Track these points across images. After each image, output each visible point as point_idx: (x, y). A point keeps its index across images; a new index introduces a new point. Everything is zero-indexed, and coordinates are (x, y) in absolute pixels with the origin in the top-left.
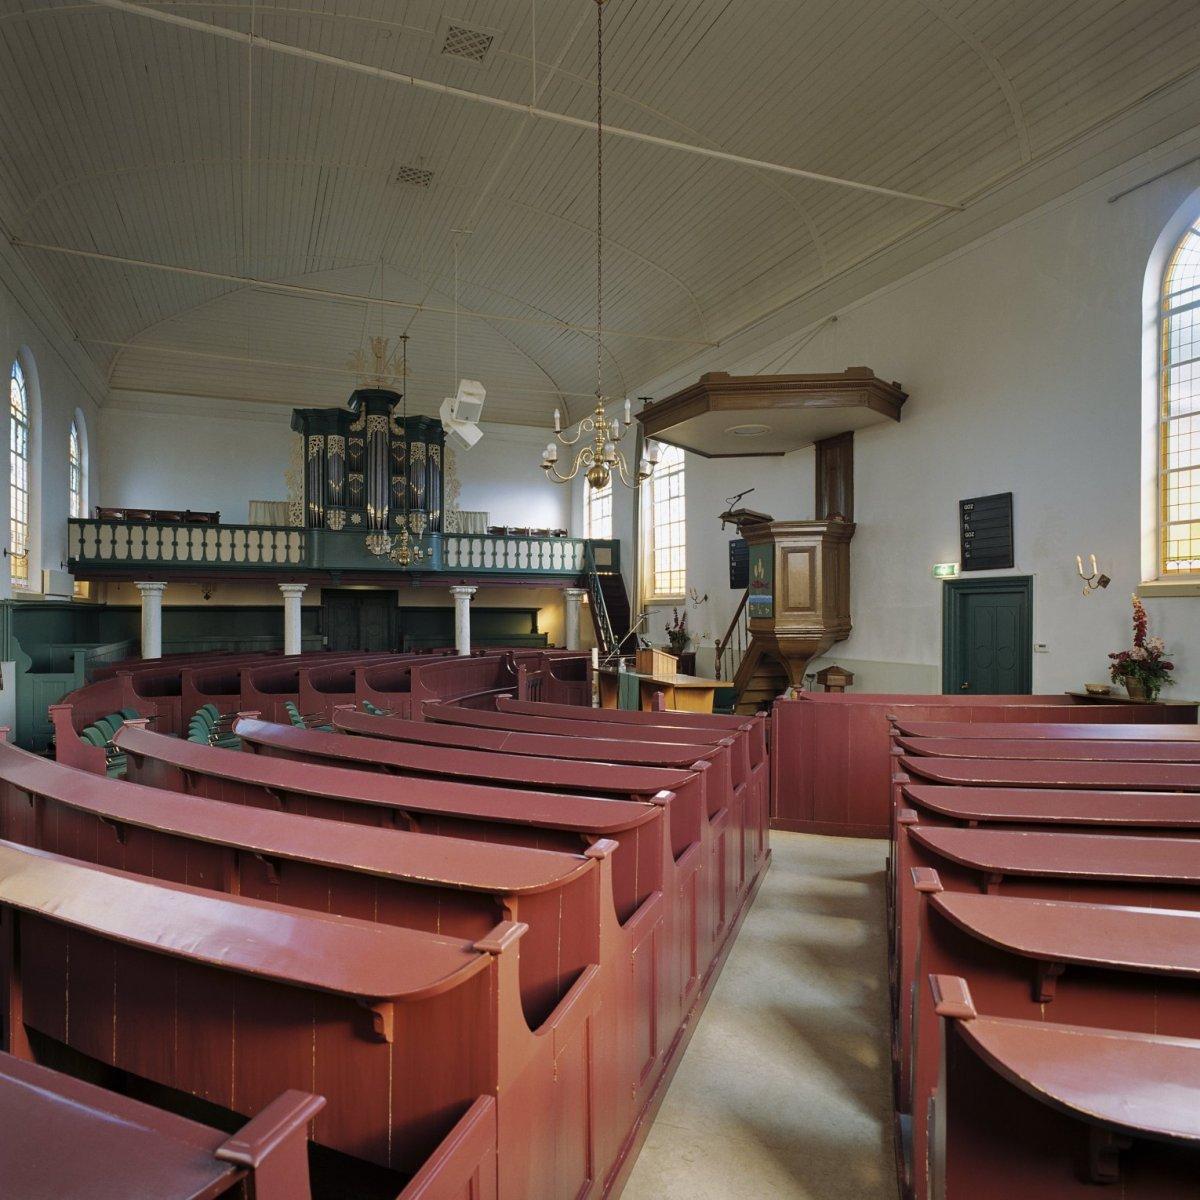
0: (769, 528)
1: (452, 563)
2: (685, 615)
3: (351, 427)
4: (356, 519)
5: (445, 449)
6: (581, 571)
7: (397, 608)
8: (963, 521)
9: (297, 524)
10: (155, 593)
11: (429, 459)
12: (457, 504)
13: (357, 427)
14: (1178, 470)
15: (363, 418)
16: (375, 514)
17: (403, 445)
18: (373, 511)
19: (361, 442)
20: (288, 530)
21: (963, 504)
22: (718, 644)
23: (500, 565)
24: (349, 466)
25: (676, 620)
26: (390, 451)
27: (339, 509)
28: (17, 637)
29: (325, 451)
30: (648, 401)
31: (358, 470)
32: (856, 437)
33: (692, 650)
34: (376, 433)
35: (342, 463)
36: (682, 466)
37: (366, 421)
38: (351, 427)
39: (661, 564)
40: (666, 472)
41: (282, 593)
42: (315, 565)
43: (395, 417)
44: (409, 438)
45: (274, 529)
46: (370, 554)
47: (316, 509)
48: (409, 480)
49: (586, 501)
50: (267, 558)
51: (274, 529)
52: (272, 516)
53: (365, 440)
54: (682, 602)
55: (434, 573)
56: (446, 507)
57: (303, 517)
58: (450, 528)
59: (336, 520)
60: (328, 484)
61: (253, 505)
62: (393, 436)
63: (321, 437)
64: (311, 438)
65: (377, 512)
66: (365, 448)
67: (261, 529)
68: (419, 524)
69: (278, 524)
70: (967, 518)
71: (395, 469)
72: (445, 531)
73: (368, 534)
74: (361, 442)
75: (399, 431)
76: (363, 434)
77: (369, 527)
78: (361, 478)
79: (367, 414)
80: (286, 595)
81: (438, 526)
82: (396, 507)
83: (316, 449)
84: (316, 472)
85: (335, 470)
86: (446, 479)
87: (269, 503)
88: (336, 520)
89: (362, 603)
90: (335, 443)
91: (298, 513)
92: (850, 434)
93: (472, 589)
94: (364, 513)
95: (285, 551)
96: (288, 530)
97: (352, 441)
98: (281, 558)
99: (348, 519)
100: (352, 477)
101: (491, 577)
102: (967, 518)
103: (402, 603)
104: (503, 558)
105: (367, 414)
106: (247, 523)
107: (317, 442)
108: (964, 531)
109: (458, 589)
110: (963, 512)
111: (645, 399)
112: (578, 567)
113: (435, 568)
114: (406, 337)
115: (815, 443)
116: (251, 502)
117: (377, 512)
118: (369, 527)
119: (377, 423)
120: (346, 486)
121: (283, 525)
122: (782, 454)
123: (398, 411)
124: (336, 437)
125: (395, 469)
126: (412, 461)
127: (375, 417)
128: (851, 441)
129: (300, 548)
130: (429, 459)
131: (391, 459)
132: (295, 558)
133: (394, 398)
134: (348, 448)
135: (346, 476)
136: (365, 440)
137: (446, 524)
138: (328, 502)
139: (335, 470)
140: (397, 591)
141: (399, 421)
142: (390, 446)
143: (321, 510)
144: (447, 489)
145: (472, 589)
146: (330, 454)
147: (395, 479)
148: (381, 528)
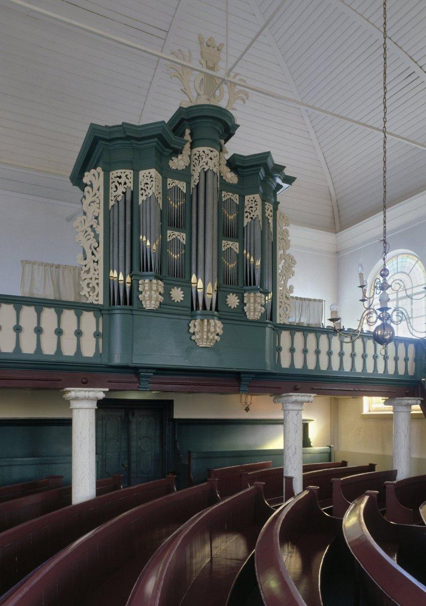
3: (171, 163)
4: (177, 294)
5: (278, 212)
9: (92, 299)
10: (261, 580)
12: (291, 288)
16: (204, 288)
17: (236, 198)
18: (200, 284)
19: (182, 186)
20: (79, 308)
24: (170, 220)
26: (220, 204)
28: (76, 186)
29: (134, 194)
31: (176, 224)
34: (206, 173)
37: (190, 156)
38: (171, 163)
41: (68, 403)
42: (117, 361)
44: (242, 189)
45: (59, 306)
47: (121, 277)
48: (242, 248)
50: (49, 349)
51: (59, 306)
52: (57, 288)
53: (188, 184)
56: (280, 288)
57: (100, 289)
60: (139, 242)
61: (28, 267)
62: (225, 185)
63: (130, 173)
64: (114, 174)
66: (188, 197)
67: (40, 304)
68: (255, 305)
69: (64, 299)
71: (230, 231)
73: (193, 317)
74: (182, 186)
75: (231, 177)
76: (185, 175)
78: (182, 237)
80: (74, 405)
81: (271, 314)
82: (225, 284)
83: (121, 189)
84: (121, 227)
85: (151, 220)
87: (52, 265)
89: (133, 415)
91: (93, 283)
94: (187, 286)
95: (75, 338)
96: (79, 308)
97: (172, 183)
98: (69, 350)
99: (167, 294)
103: (177, 415)
104: (326, 357)
106: (17, 292)
112: (411, 372)
116: (25, 263)
120: (164, 246)
121: (72, 299)
126: (246, 221)
127: (206, 149)
129: (97, 335)
132: (89, 350)
133: (85, 199)
134: (165, 191)
135: (163, 233)
136: (188, 184)
139: (151, 220)
140: (172, 401)
142: (220, 197)
143: (128, 279)
146: (141, 199)
147: (227, 244)
148: (211, 309)
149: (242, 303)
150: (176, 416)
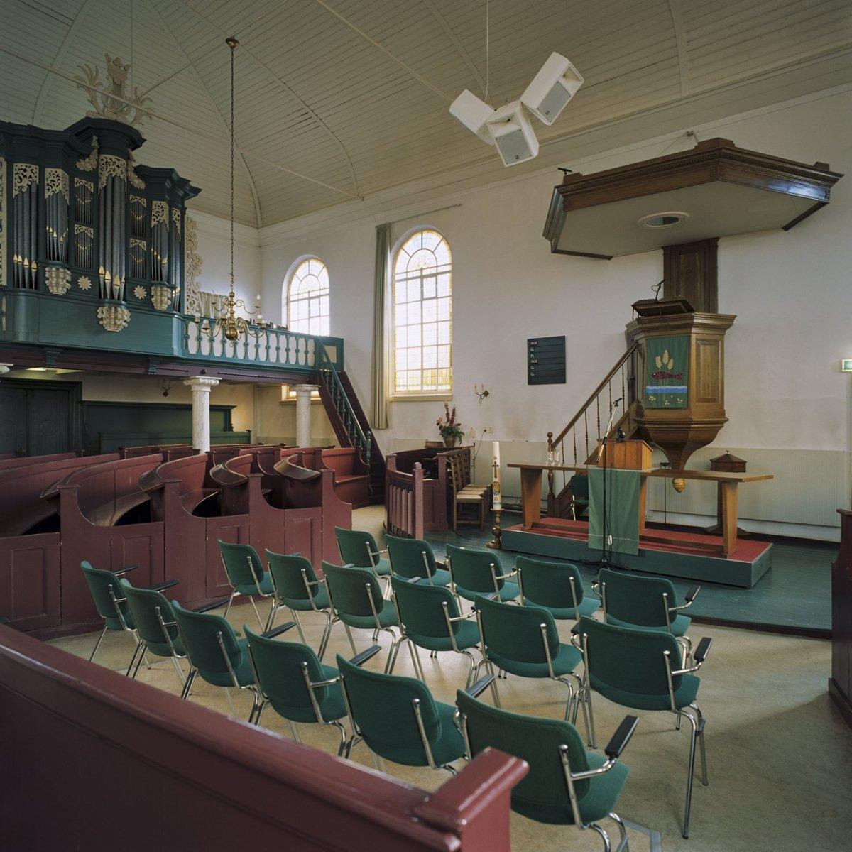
0: (692, 318)
1: (192, 349)
2: (454, 410)
3: (78, 164)
6: (312, 367)
7: (82, 403)
8: (530, 353)
11: (172, 223)
13: (86, 165)
14: (446, 344)
15: (94, 155)
16: (112, 280)
18: (108, 276)
19: (91, 187)
21: (530, 341)
22: (550, 435)
23: (273, 359)
25: (448, 414)
26: (128, 206)
27: (63, 267)
30: (568, 173)
31: (88, 223)
32: (720, 243)
33: (464, 444)
35: (66, 208)
36: (327, 291)
38: (78, 164)
39: (401, 363)
40: (306, 296)
43: (135, 165)
46: (102, 329)
47: (26, 262)
48: (149, 246)
49: (284, 302)
54: (450, 398)
55: (177, 358)
58: (191, 308)
59: (58, 281)
62: (132, 189)
65: (111, 277)
66: (96, 196)
70: (532, 350)
71: (135, 230)
72: (186, 313)
74: (91, 187)
75: (139, 183)
76: (93, 176)
77: (100, 295)
78: (90, 232)
79: (99, 153)
83: (26, 182)
85: (57, 214)
86: (187, 252)
88: (58, 281)
90: (56, 180)
92: (717, 239)
93: (215, 381)
94: (95, 277)
97: (79, 183)
99: (74, 282)
100: (79, 229)
101: (251, 370)
102: (532, 350)
105: (99, 153)
107: (28, 173)
108: (530, 359)
109: (202, 379)
110: (530, 346)
111: (565, 170)
113: (176, 354)
114: (235, 42)
115: (663, 248)
117: (111, 277)
118: (100, 295)
119: (113, 166)
120: (71, 238)
122: (609, 258)
123: (141, 157)
124: (60, 171)
125: (135, 230)
126: (153, 223)
128: (716, 247)
130: (172, 223)
131: (128, 217)
134: (72, 189)
137: (186, 304)
138: (46, 255)
139: (57, 214)
141: (141, 171)
142: (128, 200)
143: (34, 265)
144: (187, 264)
145: (215, 381)
146: (47, 194)
149: (149, 296)
150: (85, 398)
